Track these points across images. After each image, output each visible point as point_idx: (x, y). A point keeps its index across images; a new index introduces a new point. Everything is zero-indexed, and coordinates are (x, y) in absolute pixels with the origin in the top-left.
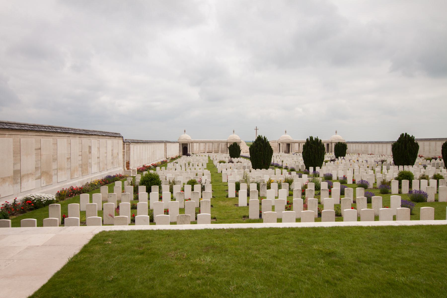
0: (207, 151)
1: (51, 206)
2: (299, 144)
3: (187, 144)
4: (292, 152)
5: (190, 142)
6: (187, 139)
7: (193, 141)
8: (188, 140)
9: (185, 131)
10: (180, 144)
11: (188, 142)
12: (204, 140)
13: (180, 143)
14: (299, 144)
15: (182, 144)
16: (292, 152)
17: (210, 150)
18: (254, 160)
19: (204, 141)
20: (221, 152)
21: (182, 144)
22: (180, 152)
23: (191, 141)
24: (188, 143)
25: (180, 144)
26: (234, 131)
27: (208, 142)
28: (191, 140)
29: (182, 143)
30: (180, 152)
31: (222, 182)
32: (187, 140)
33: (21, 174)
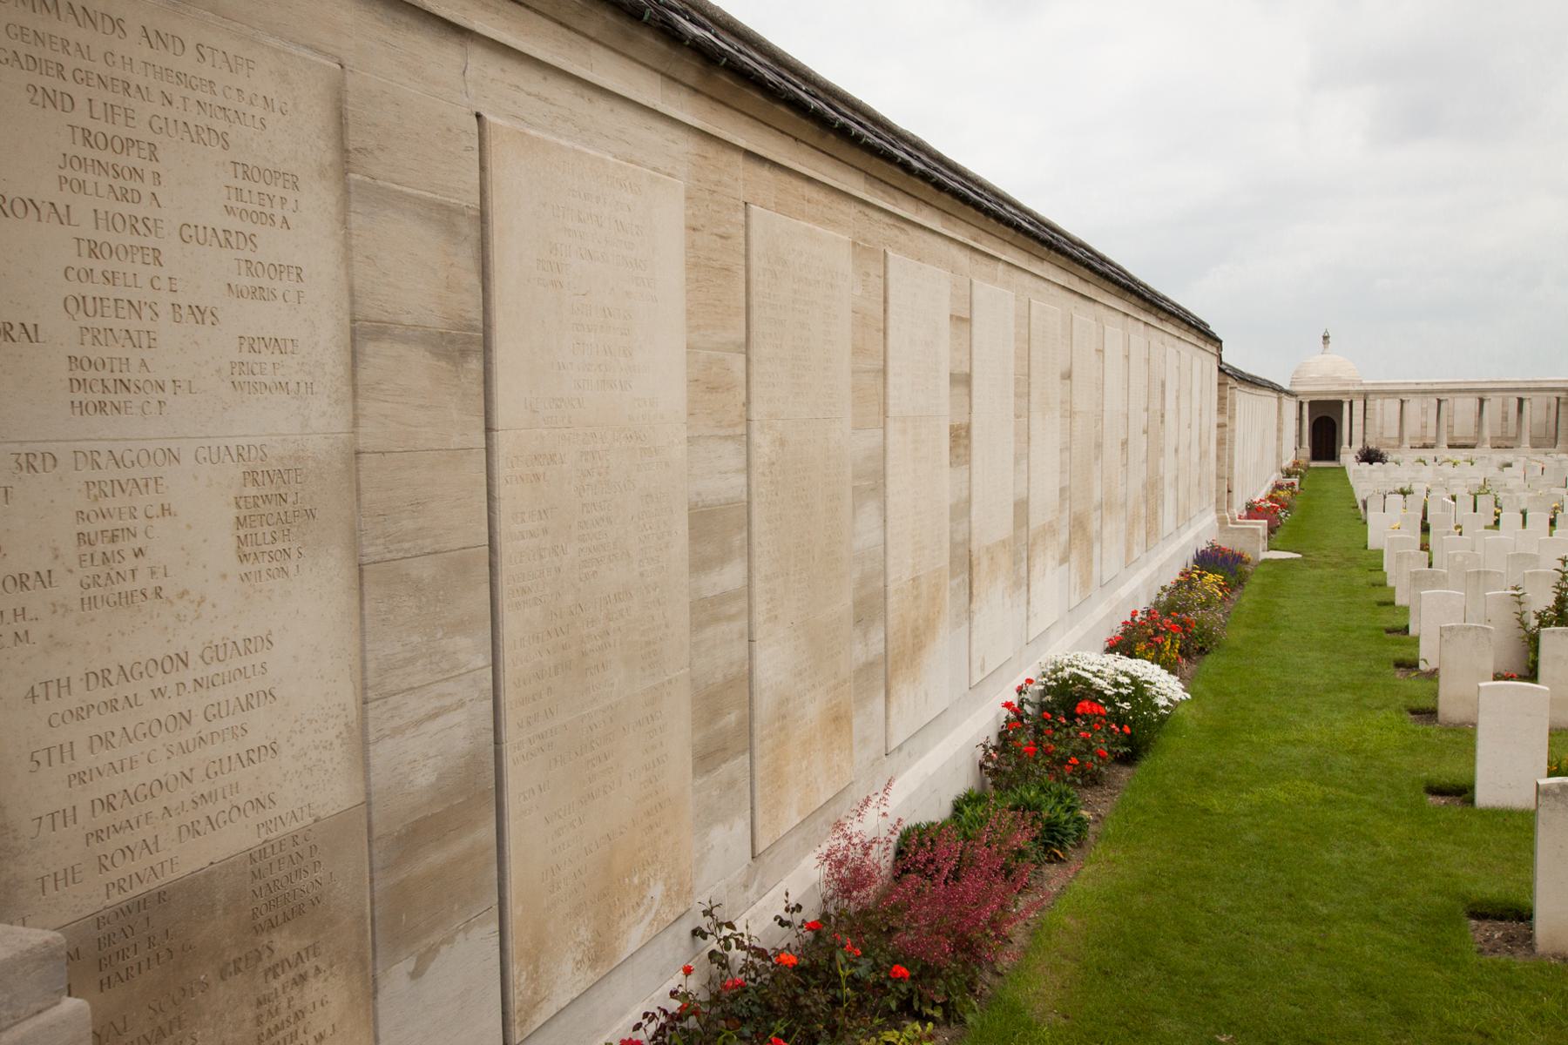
0: (1411, 438)
1: (1555, 795)
2: (1482, 401)
3: (1339, 404)
4: (1350, 444)
5: (1358, 393)
6: (1338, 379)
7: (1369, 388)
8: (1348, 384)
9: (1326, 338)
10: (1301, 404)
11: (1346, 393)
12: (1432, 384)
13: (1300, 398)
14: (1482, 401)
15: (1312, 404)
16: (1350, 444)
17: (1455, 434)
18: (298, 437)
19: (1436, 387)
20: (1534, 446)
21: (1312, 404)
22: (1300, 445)
23: (1362, 388)
24: (1346, 400)
25: (1301, 404)
26: (1326, 338)
27: (1460, 391)
28: (1362, 384)
29: (1315, 398)
30: (1300, 445)
31: (1393, 603)
32: (1340, 385)
33: (1031, 527)
